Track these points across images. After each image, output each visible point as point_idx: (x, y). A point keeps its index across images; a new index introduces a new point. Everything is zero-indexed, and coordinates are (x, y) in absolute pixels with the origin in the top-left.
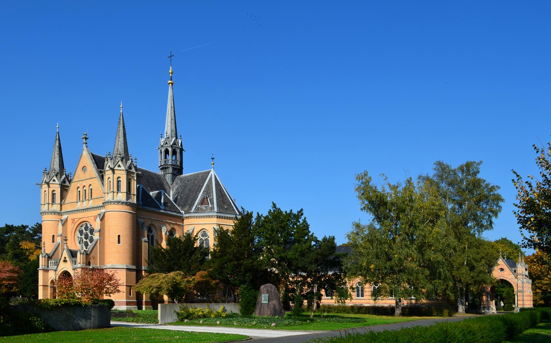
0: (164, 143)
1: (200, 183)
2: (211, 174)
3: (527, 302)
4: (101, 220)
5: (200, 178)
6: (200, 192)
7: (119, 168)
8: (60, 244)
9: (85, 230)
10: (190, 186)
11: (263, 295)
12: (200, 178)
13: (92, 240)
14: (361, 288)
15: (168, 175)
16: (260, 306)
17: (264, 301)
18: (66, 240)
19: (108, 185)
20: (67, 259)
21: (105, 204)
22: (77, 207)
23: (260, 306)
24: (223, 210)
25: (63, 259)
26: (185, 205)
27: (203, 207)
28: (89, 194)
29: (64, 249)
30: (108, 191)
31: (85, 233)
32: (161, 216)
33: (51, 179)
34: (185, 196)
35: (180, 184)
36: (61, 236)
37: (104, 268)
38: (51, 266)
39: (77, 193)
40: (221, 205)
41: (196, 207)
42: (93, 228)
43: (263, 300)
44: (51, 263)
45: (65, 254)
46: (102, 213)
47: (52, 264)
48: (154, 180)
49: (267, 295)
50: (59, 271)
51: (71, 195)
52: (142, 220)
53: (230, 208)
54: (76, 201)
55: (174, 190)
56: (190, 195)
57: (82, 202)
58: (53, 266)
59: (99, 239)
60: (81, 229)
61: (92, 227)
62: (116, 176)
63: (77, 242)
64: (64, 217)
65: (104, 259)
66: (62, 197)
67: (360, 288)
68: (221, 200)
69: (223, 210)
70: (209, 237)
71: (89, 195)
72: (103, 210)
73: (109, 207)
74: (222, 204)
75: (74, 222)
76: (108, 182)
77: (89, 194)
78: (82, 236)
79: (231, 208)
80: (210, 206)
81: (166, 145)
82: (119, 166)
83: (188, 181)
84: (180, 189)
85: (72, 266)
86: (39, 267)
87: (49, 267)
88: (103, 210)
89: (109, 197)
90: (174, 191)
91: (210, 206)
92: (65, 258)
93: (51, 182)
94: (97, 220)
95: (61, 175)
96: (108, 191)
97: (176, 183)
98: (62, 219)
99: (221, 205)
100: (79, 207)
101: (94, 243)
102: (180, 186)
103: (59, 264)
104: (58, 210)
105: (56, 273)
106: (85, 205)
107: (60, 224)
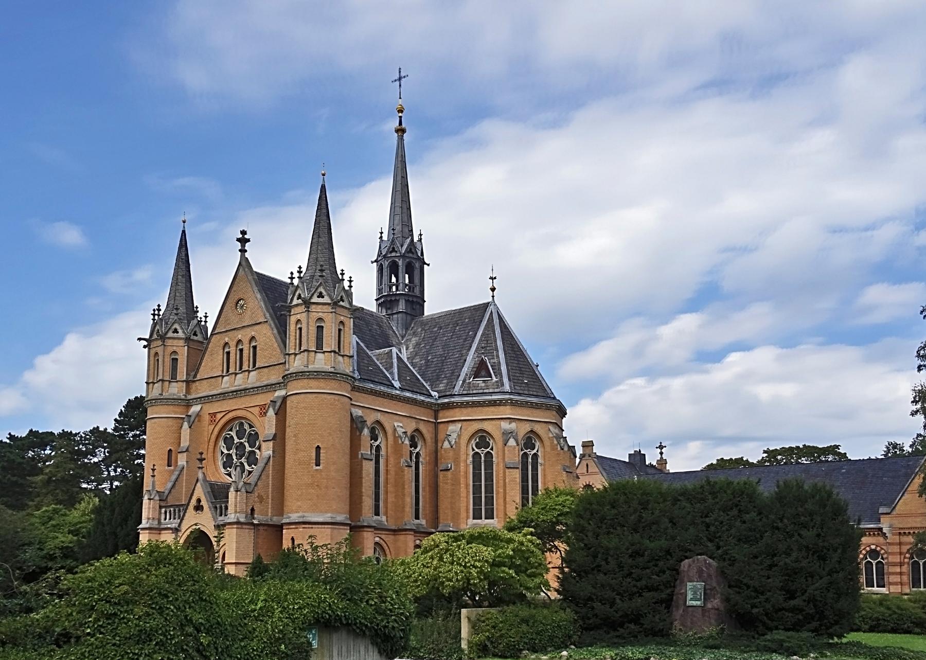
0: (388, 249)
1: (467, 331)
2: (490, 312)
3: (895, 580)
4: (276, 414)
5: (467, 320)
6: (469, 350)
7: (320, 300)
8: (183, 468)
9: (238, 438)
10: (446, 338)
11: (689, 585)
12: (467, 320)
13: (253, 460)
14: (877, 564)
15: (395, 316)
16: (681, 611)
17: (691, 599)
18: (201, 460)
19: (296, 336)
20: (204, 503)
21: (287, 378)
22: (223, 386)
23: (681, 611)
24: (522, 388)
25: (193, 502)
26: (438, 379)
27: (479, 381)
28: (249, 357)
29: (197, 481)
30: (295, 349)
31: (238, 444)
32: (394, 402)
33: (170, 329)
34: (436, 359)
35: (421, 334)
36: (187, 450)
37: (284, 521)
38: (165, 519)
39: (250, 350)
40: (515, 378)
41: (464, 381)
42: (257, 433)
43: (689, 596)
44: (166, 512)
45: (200, 492)
46: (278, 397)
47: (168, 514)
48: (370, 328)
49: (700, 585)
50: (183, 531)
51: (212, 364)
52: (360, 412)
53: (534, 382)
54: (220, 373)
55: (411, 347)
56: (447, 357)
57: (234, 375)
58: (170, 519)
59: (273, 457)
60: (229, 434)
61: (254, 431)
62: (315, 316)
63: (220, 464)
64: (195, 409)
65: (361, 503)
66: (194, 368)
67: (874, 564)
68: (515, 365)
69: (522, 388)
70: (492, 449)
71: (249, 361)
72: (281, 393)
73: (295, 387)
74: (518, 375)
75: (215, 421)
76: (296, 330)
77: (249, 357)
78: (232, 451)
79: (536, 384)
80: (495, 379)
81: (393, 254)
82: (321, 296)
83: (441, 328)
84: (423, 345)
85: (215, 519)
86: (140, 523)
87: (162, 521)
88: (281, 393)
89: (297, 364)
90: (411, 349)
91: (495, 379)
92: (199, 501)
93: (170, 334)
94: (268, 414)
95: (189, 319)
96: (295, 349)
97: (414, 333)
98: (189, 414)
99: (515, 378)
100: (227, 386)
101: (261, 464)
102: (423, 338)
103: (184, 515)
104: (182, 394)
105: (177, 536)
106: (240, 381)
107: (186, 425)
